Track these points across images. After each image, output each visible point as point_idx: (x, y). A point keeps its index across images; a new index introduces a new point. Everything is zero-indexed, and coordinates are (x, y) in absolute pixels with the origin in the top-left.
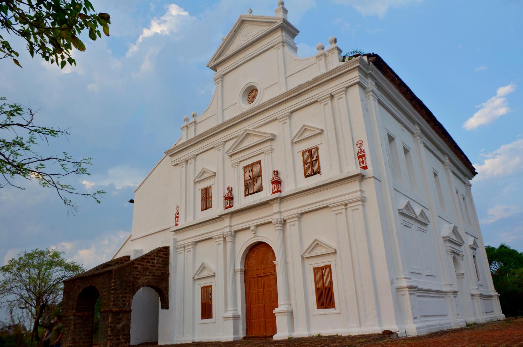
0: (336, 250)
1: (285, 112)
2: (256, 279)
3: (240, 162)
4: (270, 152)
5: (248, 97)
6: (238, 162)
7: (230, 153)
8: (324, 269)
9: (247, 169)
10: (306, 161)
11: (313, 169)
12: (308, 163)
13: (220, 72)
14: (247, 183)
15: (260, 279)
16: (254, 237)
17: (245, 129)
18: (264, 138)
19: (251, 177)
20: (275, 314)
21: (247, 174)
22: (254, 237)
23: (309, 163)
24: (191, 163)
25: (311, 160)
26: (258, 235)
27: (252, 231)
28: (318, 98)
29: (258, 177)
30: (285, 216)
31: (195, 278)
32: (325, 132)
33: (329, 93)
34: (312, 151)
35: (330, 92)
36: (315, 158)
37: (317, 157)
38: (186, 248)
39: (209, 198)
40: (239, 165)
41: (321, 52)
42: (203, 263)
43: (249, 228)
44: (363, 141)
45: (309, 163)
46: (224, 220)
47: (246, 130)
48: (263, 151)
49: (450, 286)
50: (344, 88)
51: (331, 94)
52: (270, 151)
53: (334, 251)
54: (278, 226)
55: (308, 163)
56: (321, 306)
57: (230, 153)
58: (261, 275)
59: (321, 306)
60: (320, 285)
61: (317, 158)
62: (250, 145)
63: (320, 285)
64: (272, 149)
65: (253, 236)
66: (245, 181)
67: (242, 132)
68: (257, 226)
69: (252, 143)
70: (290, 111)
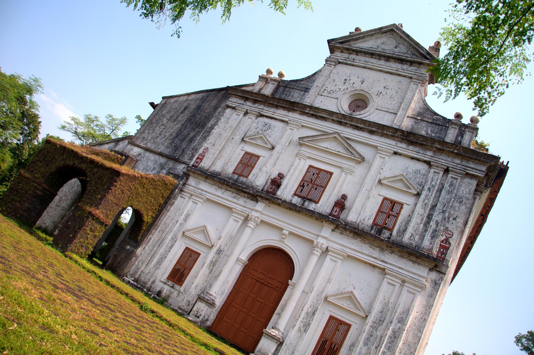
0: (213, 246)
2: (254, 281)
3: (309, 157)
5: (354, 101)
9: (312, 170)
10: (306, 179)
12: (384, 213)
13: (338, 58)
14: (304, 183)
15: (259, 284)
17: (336, 131)
19: (312, 181)
20: (263, 333)
23: (386, 213)
24: (249, 118)
25: (389, 212)
26: (285, 242)
29: (321, 186)
31: (328, 299)
33: (447, 165)
35: (449, 165)
36: (394, 213)
37: (397, 214)
38: (193, 197)
39: (249, 166)
43: (281, 229)
45: (386, 213)
46: (257, 202)
48: (343, 166)
51: (448, 168)
53: (211, 246)
55: (384, 213)
58: (262, 281)
60: (328, 336)
61: (396, 215)
62: (331, 149)
63: (328, 336)
66: (303, 180)
69: (333, 149)
70: (395, 150)
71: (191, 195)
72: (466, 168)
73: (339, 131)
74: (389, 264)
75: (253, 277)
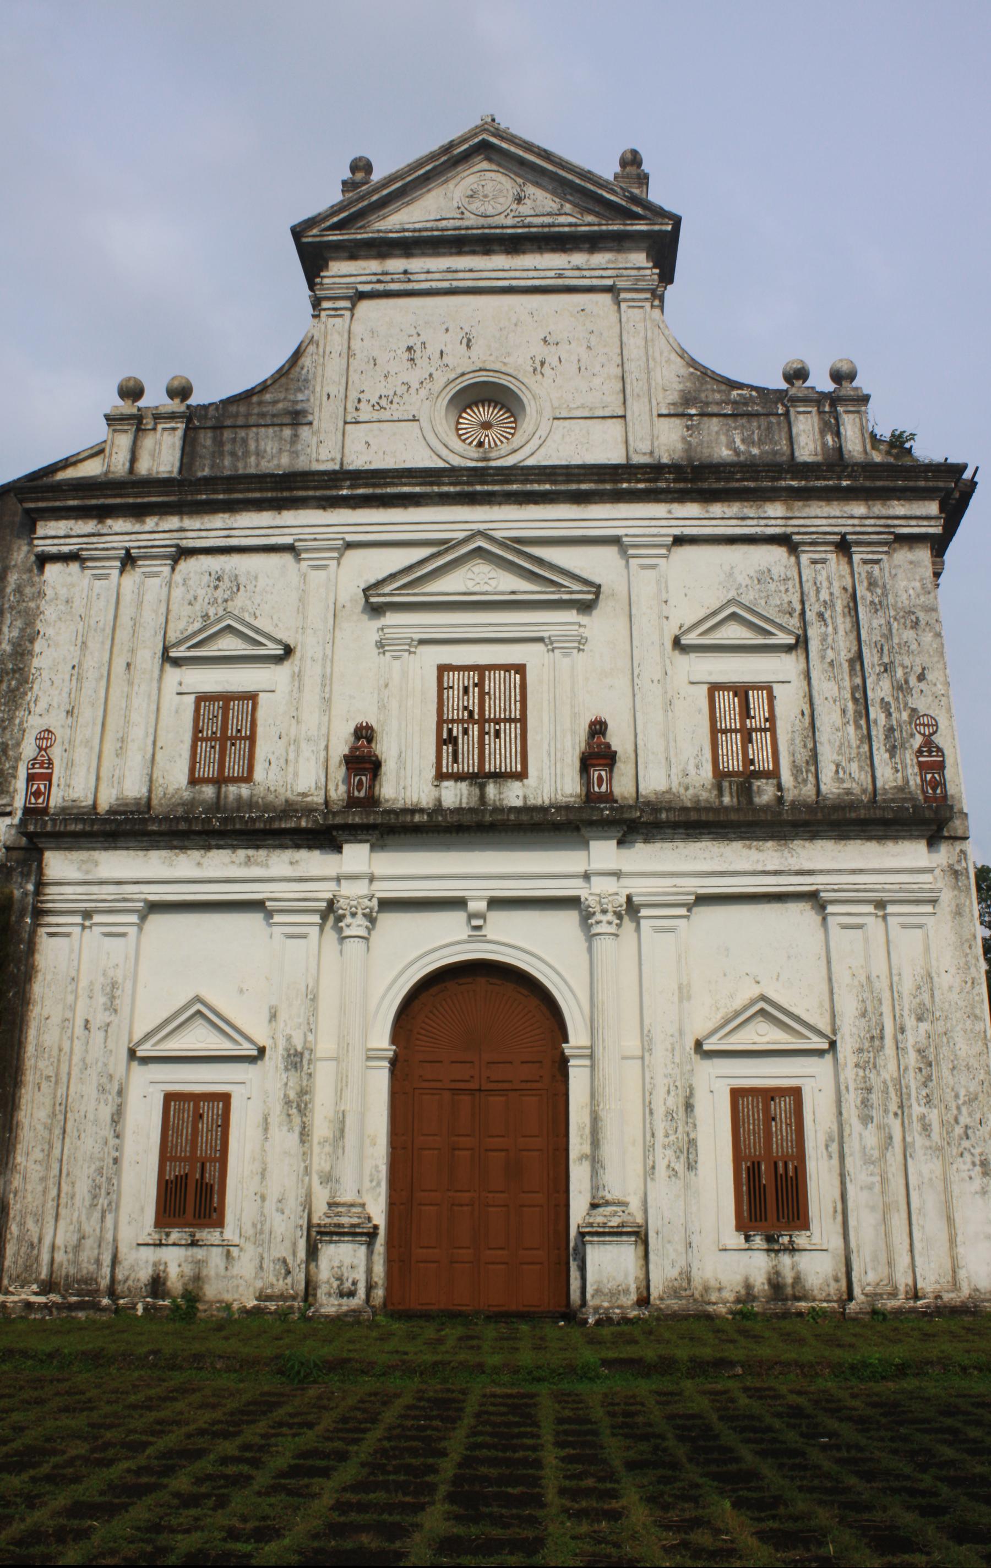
1: (663, 531)
3: (422, 642)
4: (574, 648)
6: (412, 640)
7: (384, 595)
8: (773, 1099)
11: (751, 757)
16: (471, 939)
18: (585, 589)
19: (471, 713)
21: (454, 699)
22: (471, 939)
26: (490, 937)
27: (471, 917)
28: (798, 533)
30: (639, 888)
32: (298, 654)
34: (751, 698)
37: (766, 720)
39: (236, 738)
40: (414, 653)
41: (126, 407)
42: (271, 1008)
43: (458, 903)
44: (937, 718)
47: (481, 533)
48: (545, 635)
49: (68, 1174)
50: (341, 542)
52: (407, 647)
54: (610, 923)
56: (756, 1220)
57: (384, 595)
59: (199, 1217)
60: (755, 1147)
64: (583, 641)
65: (469, 936)
66: (441, 721)
67: (461, 535)
68: (496, 903)
70: (677, 531)
71: (87, 914)
72: (890, 522)
73: (482, 527)
74: (821, 872)
75: (506, 1086)
